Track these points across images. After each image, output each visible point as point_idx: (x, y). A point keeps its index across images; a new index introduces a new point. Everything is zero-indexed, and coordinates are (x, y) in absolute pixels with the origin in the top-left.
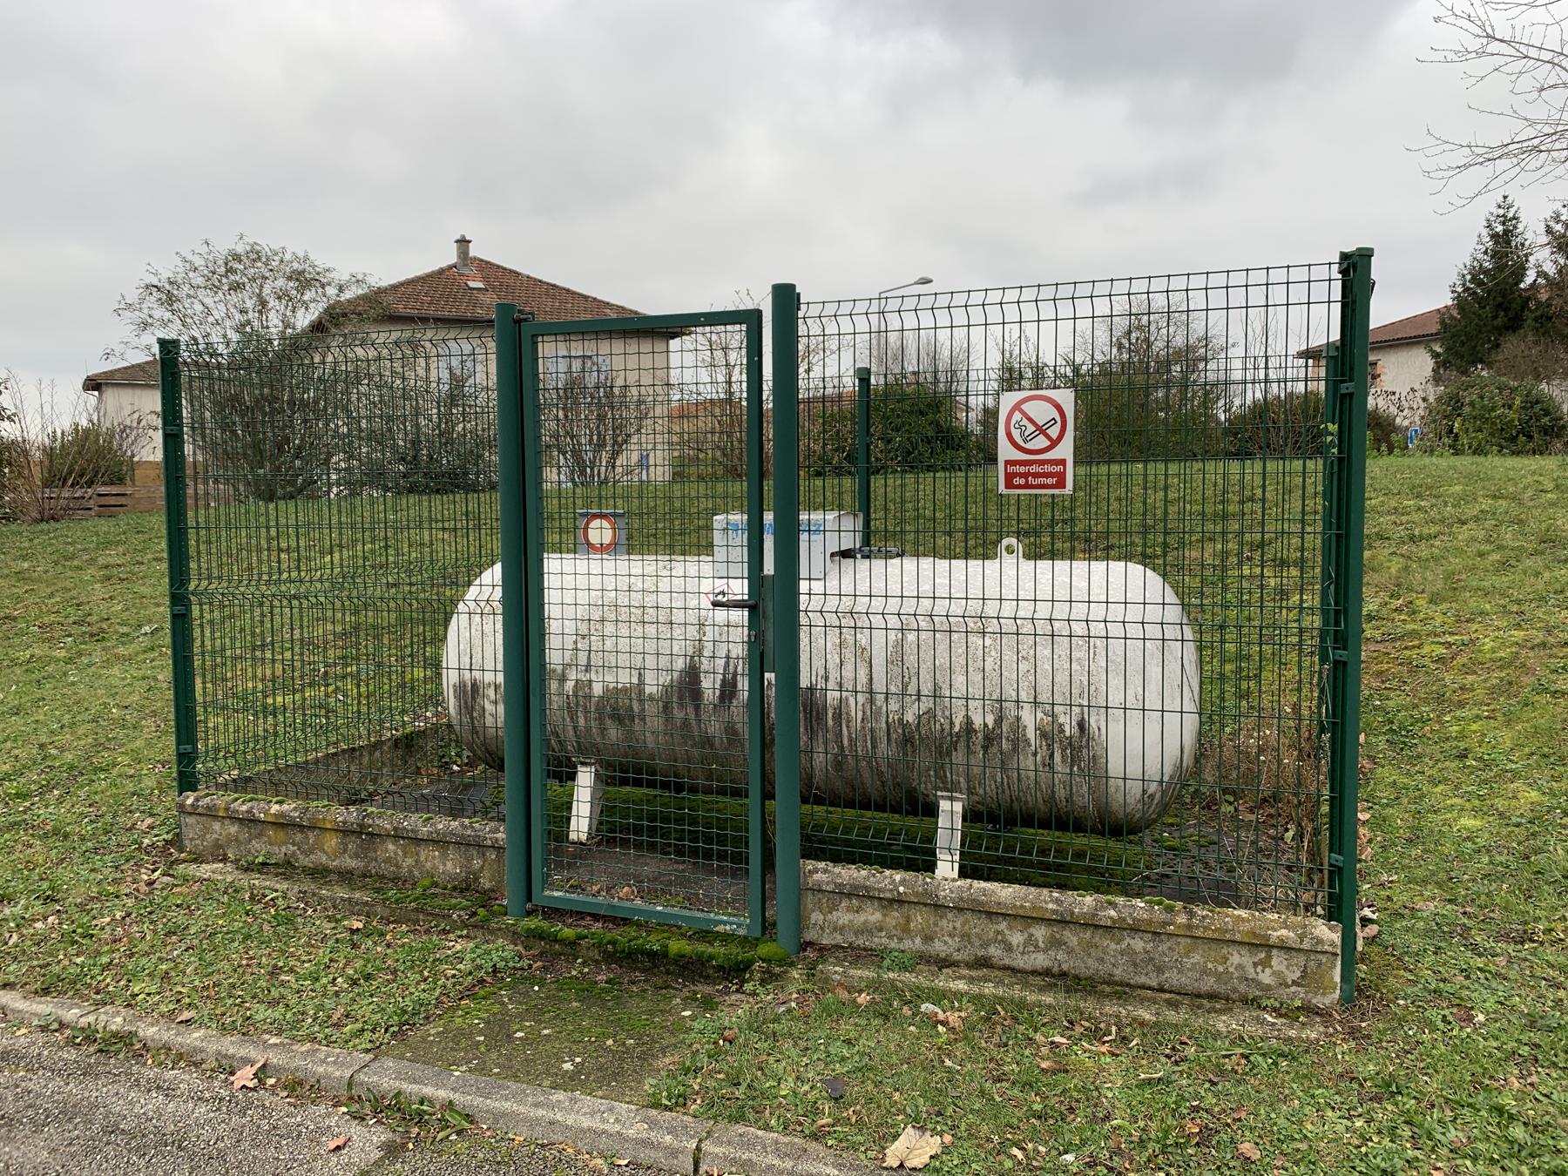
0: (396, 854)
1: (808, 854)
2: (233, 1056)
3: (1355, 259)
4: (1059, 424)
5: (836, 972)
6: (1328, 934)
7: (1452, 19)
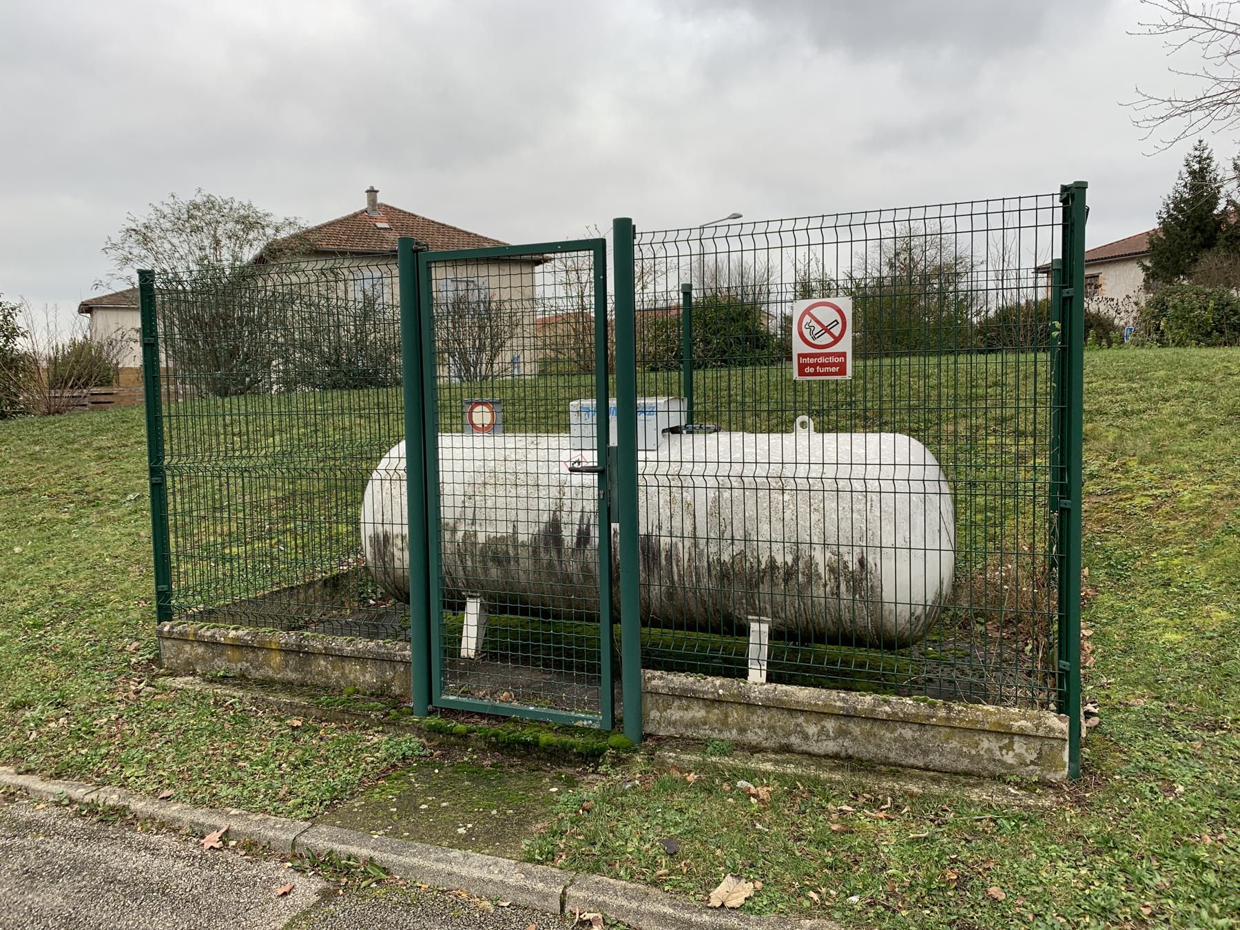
0: (326, 668)
4: (840, 325)
5: (670, 757)
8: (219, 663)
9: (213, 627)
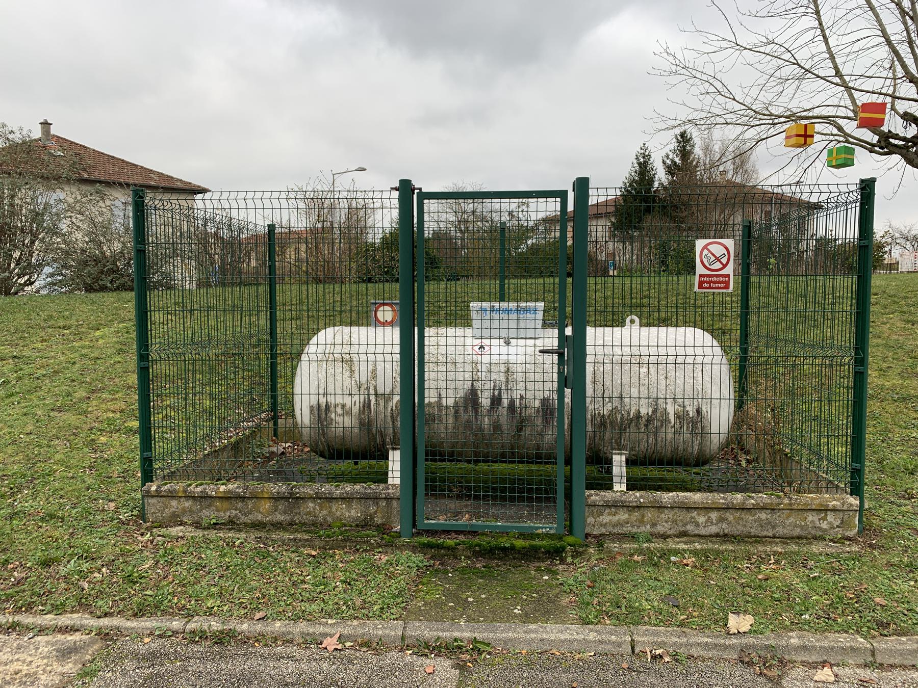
0: (314, 509)
1: (589, 487)
2: (314, 634)
3: (868, 182)
4: (727, 257)
5: (615, 547)
6: (854, 501)
7: (665, 55)
8: (208, 514)
9: (201, 484)
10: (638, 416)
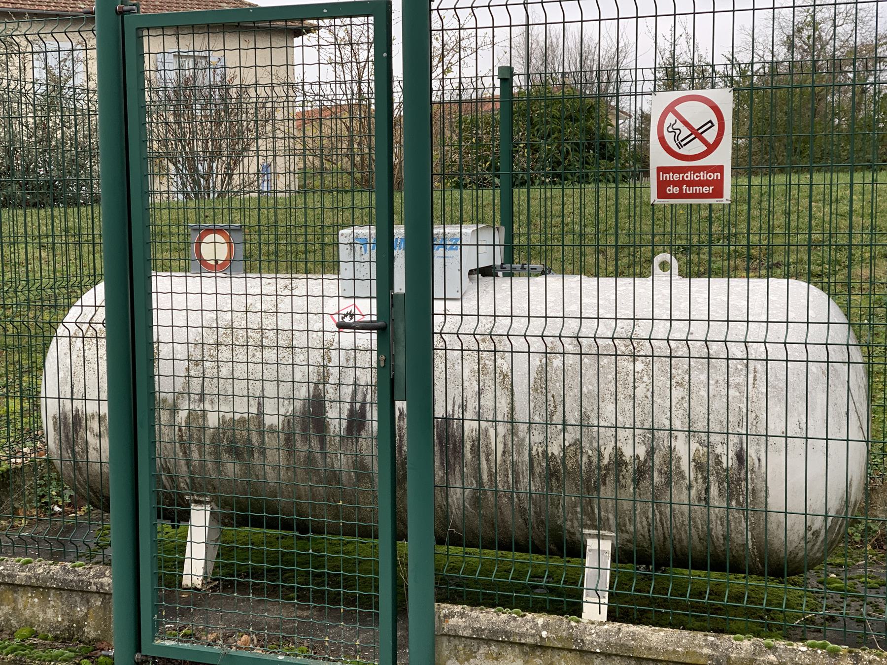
1: (445, 597)
4: (716, 128)
10: (618, 460)
